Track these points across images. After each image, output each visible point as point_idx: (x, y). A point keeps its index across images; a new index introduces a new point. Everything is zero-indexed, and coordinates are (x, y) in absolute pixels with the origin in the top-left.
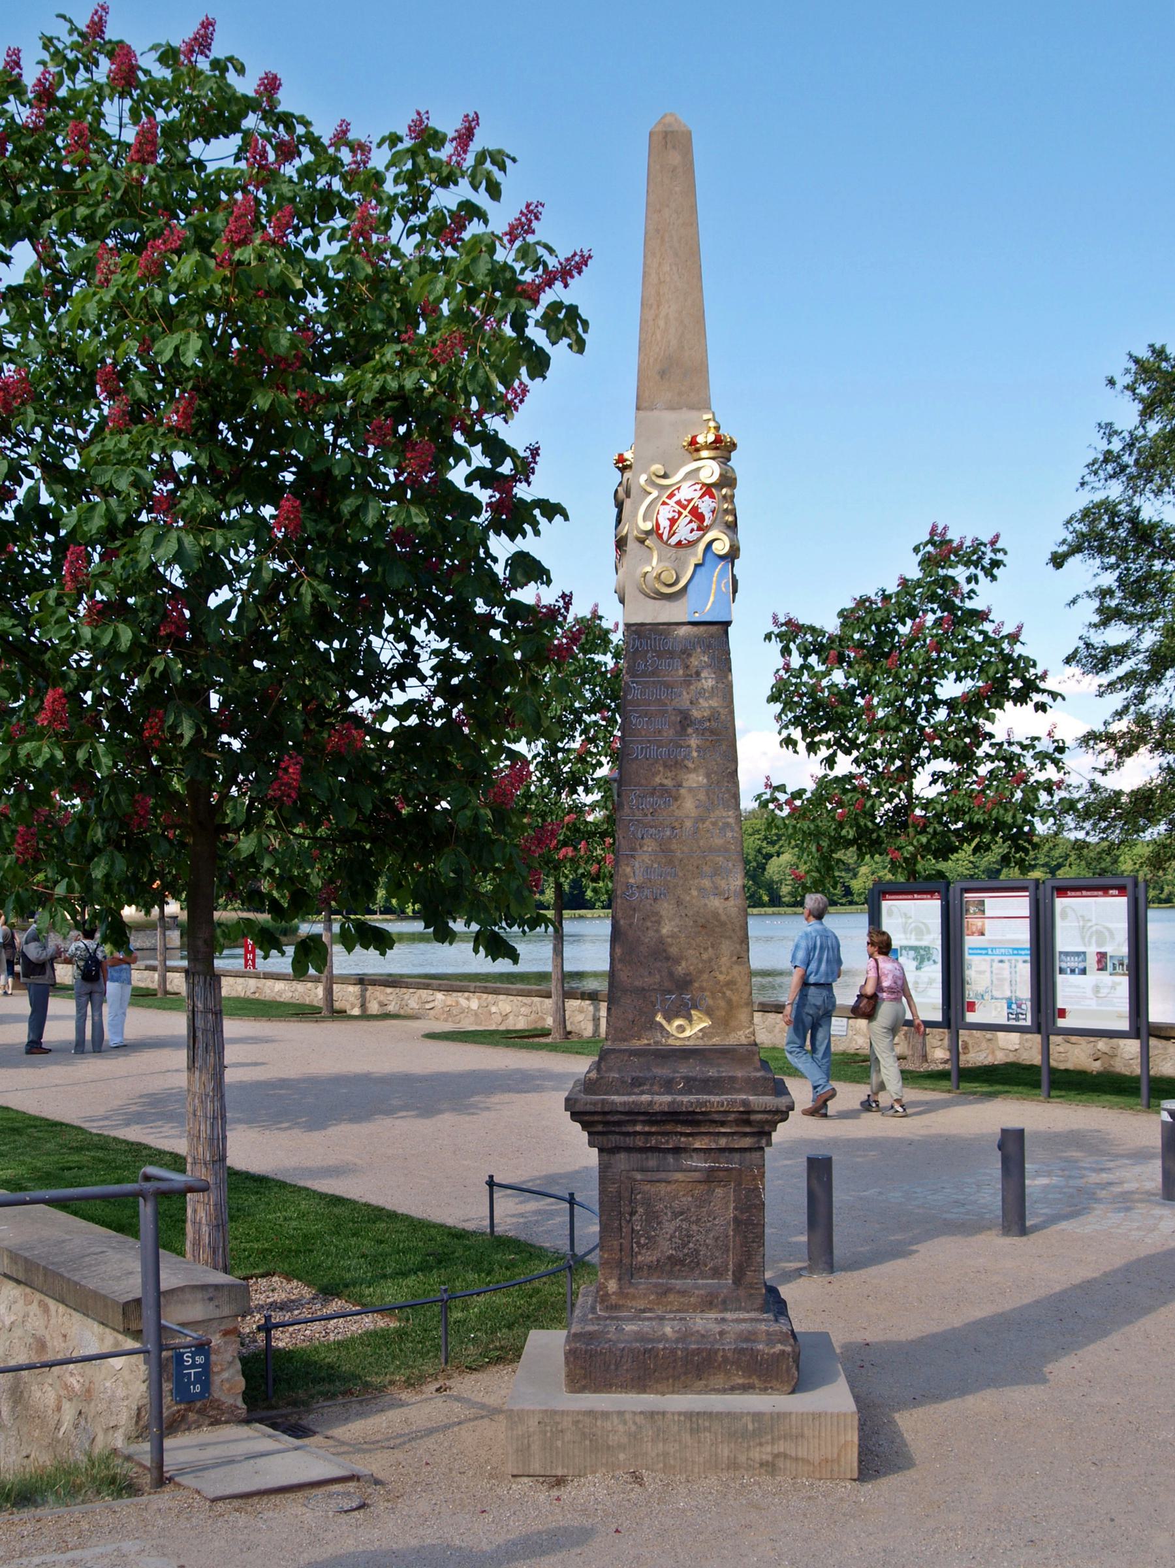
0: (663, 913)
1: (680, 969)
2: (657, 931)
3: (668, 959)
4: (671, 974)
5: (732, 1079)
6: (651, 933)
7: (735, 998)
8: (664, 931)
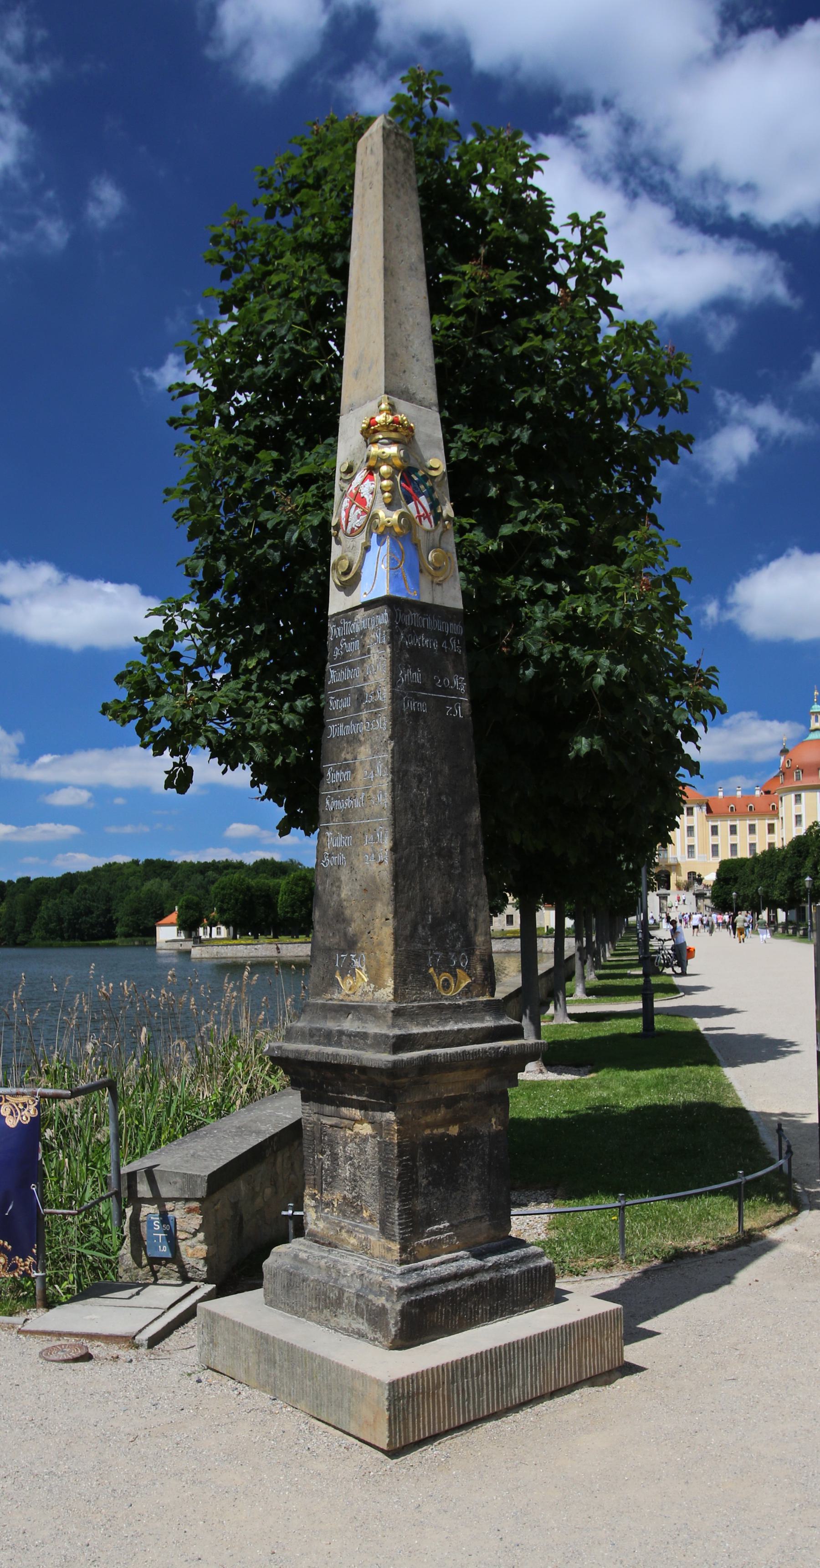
0: (343, 878)
1: (351, 930)
2: (339, 895)
3: (344, 920)
4: (345, 934)
5: (364, 1036)
6: (335, 897)
7: (382, 958)
8: (343, 896)
